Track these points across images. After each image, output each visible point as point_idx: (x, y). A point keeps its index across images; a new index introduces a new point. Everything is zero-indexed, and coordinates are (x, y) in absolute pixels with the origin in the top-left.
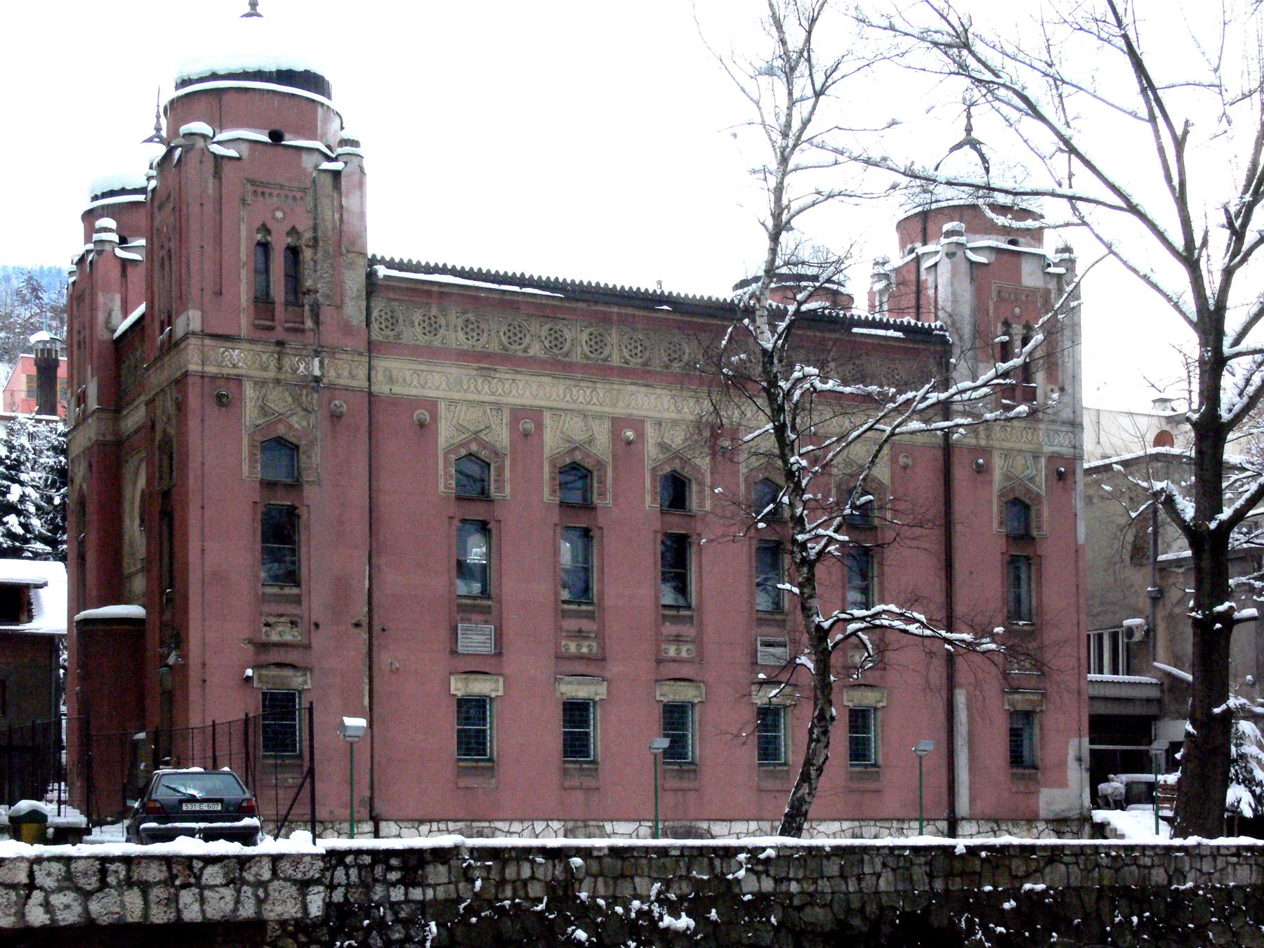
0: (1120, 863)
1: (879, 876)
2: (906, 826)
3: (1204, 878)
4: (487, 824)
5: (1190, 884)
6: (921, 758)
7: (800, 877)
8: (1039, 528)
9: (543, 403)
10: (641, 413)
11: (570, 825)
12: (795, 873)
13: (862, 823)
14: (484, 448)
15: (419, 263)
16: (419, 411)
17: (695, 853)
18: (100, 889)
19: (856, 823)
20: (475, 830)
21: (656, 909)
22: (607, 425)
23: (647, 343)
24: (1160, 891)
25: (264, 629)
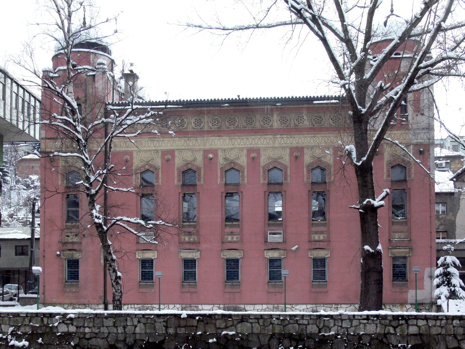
0: (286, 322)
1: (136, 326)
2: (339, 306)
3: (343, 330)
4: (150, 305)
5: (332, 333)
6: (159, 278)
7: (91, 326)
8: (410, 176)
9: (175, 148)
10: (217, 147)
11: (184, 306)
12: (88, 324)
13: (317, 305)
14: (151, 167)
15: (160, 101)
16: (127, 156)
17: (34, 315)
18: (216, 328)
19: (314, 306)
20: (145, 308)
21: (10, 337)
22: (202, 153)
23: (220, 119)
24: (310, 336)
25: (66, 237)
